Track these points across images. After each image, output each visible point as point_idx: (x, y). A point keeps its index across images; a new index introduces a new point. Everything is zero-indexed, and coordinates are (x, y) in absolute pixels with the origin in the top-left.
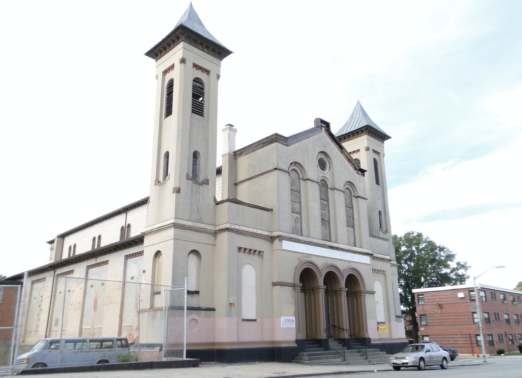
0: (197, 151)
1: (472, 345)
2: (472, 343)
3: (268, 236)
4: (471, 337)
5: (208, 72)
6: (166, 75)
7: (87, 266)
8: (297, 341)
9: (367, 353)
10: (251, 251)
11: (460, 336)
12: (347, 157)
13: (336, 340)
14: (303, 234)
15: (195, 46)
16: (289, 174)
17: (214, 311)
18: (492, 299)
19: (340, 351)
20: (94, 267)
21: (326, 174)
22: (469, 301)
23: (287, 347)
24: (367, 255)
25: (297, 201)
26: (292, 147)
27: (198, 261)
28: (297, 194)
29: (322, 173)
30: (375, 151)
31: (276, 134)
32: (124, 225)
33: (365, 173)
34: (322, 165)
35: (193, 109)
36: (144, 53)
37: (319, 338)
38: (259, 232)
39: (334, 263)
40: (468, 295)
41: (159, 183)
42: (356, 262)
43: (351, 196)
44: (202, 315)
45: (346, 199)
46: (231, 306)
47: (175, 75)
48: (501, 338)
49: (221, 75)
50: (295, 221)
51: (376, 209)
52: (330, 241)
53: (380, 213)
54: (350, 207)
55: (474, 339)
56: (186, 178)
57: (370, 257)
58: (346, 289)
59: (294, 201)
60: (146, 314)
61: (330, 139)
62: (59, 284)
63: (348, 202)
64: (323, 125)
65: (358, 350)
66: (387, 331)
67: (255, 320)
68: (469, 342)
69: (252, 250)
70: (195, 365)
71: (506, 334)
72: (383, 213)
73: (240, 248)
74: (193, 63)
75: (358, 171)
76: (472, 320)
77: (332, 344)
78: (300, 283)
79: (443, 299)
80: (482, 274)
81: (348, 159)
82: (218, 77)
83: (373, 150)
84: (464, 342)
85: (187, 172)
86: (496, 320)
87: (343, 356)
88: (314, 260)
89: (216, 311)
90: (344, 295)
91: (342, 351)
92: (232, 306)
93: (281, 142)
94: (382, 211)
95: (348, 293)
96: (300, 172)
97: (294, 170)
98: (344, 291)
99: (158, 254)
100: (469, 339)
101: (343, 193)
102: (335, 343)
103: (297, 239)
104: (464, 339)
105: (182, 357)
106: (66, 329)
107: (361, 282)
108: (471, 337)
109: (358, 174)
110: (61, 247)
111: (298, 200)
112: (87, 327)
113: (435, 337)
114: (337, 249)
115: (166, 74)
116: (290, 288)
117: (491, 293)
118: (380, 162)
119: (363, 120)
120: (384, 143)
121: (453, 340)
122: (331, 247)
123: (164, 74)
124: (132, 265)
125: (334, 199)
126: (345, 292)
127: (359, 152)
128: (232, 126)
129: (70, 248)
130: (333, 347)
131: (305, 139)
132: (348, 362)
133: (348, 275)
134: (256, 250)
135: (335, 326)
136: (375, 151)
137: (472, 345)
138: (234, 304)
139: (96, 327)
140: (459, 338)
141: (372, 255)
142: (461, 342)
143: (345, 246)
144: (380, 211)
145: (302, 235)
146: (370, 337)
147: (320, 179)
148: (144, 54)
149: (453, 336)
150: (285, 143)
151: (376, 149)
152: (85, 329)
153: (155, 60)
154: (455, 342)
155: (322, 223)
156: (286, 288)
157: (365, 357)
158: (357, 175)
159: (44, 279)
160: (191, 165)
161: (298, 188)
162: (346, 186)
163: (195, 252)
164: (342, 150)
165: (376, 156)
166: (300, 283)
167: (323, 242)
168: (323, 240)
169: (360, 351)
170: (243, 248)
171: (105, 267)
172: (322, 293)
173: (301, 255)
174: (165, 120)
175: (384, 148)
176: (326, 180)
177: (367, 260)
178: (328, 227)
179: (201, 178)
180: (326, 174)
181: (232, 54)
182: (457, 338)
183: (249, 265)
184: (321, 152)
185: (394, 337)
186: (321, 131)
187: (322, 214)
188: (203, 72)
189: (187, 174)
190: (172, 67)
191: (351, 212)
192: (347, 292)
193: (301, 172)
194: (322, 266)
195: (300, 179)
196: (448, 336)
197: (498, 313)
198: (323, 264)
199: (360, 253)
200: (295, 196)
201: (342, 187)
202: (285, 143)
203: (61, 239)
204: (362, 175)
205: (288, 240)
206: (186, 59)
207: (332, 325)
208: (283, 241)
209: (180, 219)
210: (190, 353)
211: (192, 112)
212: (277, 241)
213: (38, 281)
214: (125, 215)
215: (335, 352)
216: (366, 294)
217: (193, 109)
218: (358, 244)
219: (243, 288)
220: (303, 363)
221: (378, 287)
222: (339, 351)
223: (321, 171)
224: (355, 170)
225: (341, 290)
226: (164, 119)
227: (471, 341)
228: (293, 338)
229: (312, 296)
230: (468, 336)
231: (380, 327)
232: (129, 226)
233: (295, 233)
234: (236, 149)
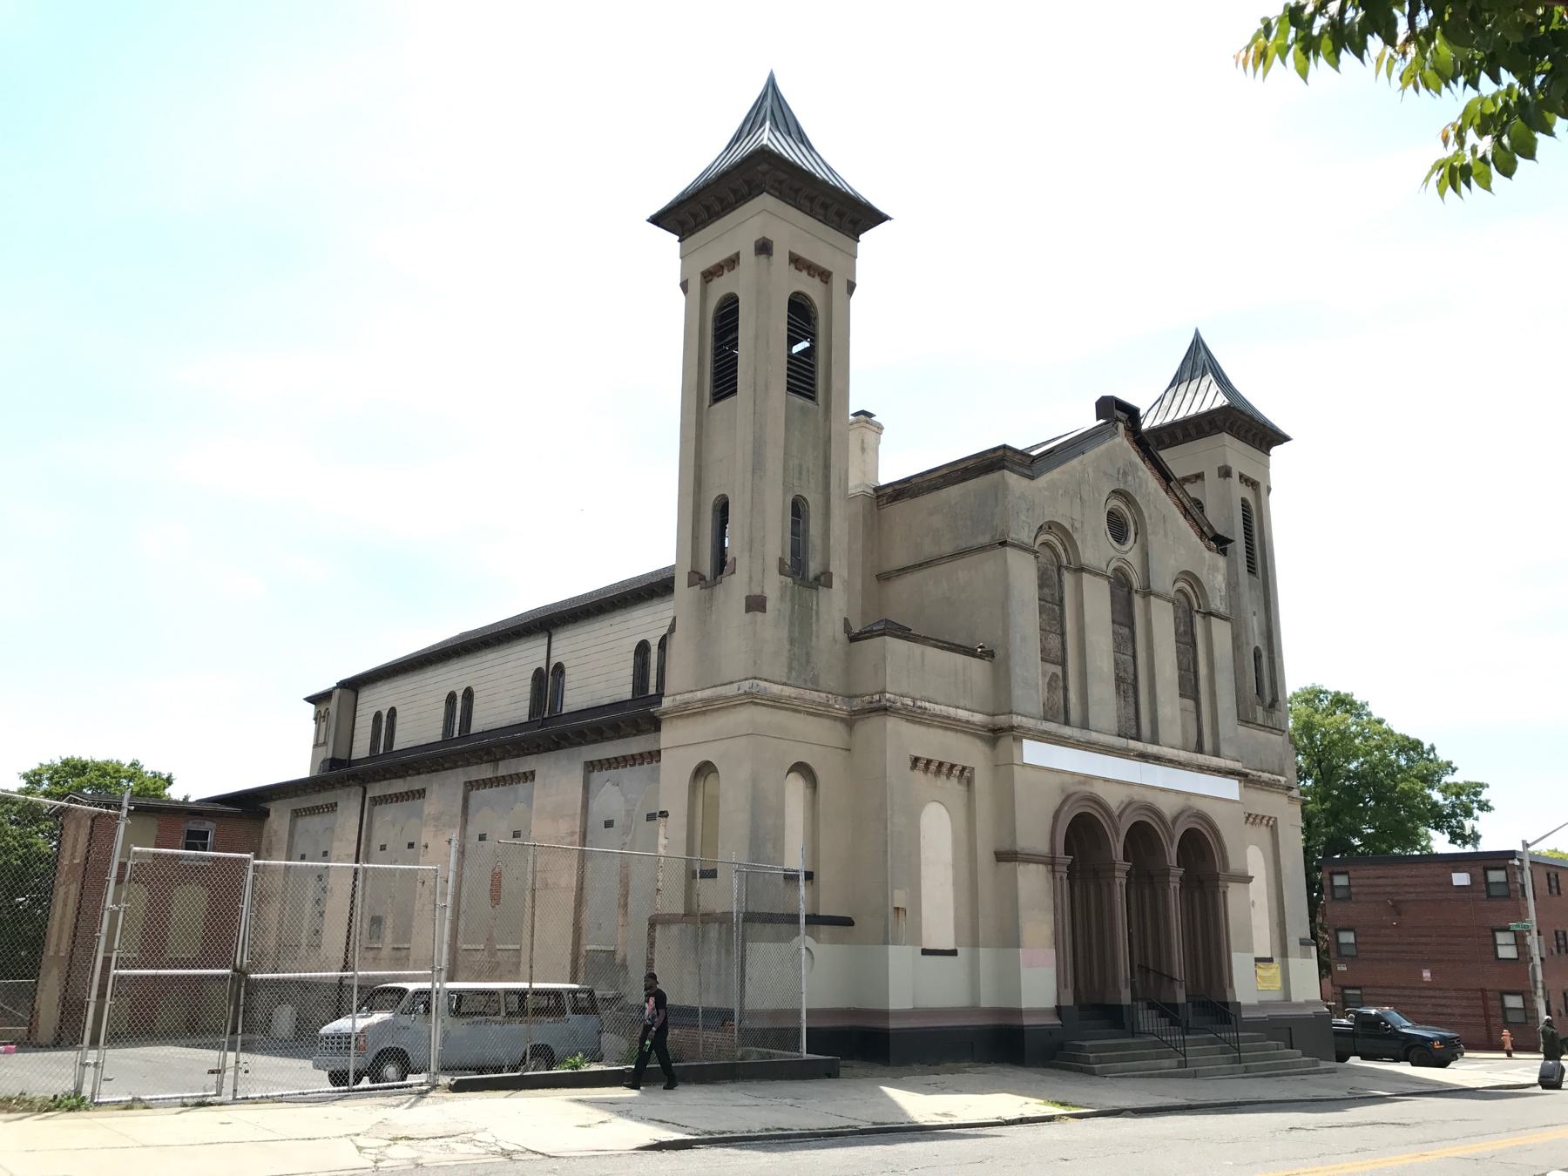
0: (802, 497)
1: (1488, 1022)
2: (1487, 1016)
3: (983, 727)
4: (1484, 998)
6: (710, 284)
7: (465, 783)
8: (1059, 1010)
9: (1238, 1043)
12: (1181, 502)
14: (1071, 719)
15: (793, 203)
16: (1037, 557)
17: (850, 927)
18: (1550, 892)
19: (1173, 1038)
20: (489, 785)
21: (1127, 552)
22: (1484, 896)
24: (1233, 777)
25: (1053, 630)
27: (808, 791)
28: (1053, 610)
31: (1005, 447)
32: (543, 665)
34: (1118, 527)
37: (841, 946)
38: (963, 714)
39: (1150, 797)
40: (1481, 879)
41: (700, 580)
42: (1205, 796)
43: (1191, 613)
44: (822, 936)
45: (1177, 620)
46: (898, 917)
49: (857, 282)
50: (1049, 684)
51: (1248, 644)
52: (1138, 738)
53: (1257, 656)
54: (1186, 640)
55: (1497, 1003)
57: (1240, 781)
60: (675, 929)
61: (1138, 452)
62: (377, 824)
63: (1182, 629)
64: (1119, 414)
66: (1278, 984)
67: (953, 953)
70: (830, 1073)
72: (1264, 654)
74: (790, 252)
75: (1209, 539)
76: (1492, 949)
77: (1147, 1019)
78: (1066, 855)
79: (1407, 889)
80: (1551, 833)
81: (1182, 509)
82: (851, 287)
83: (1241, 476)
86: (1559, 951)
88: (1100, 790)
89: (855, 927)
91: (1173, 1038)
93: (1016, 468)
94: (1261, 648)
96: (1062, 551)
97: (1044, 544)
99: (704, 770)
100: (1480, 1002)
101: (1171, 604)
103: (1058, 736)
104: (1464, 1003)
105: (797, 1049)
106: (406, 946)
107: (1218, 855)
108: (1484, 998)
109: (1209, 549)
110: (352, 714)
111: (1056, 628)
112: (469, 947)
113: (1380, 991)
114: (1158, 759)
115: (711, 280)
116: (1042, 867)
117: (1548, 875)
118: (1259, 508)
121: (1433, 1005)
122: (1144, 757)
123: (705, 278)
124: (604, 788)
126: (1178, 880)
127: (1199, 482)
128: (869, 415)
129: (378, 716)
130: (1146, 1025)
131: (1075, 457)
132: (1195, 1071)
133: (1185, 832)
134: (956, 765)
135: (1148, 970)
136: (1244, 479)
138: (904, 910)
139: (498, 947)
140: (1450, 998)
141: (1246, 775)
142: (1457, 1011)
143: (1176, 752)
145: (1067, 723)
146: (1238, 1000)
148: (648, 220)
149: (1431, 993)
152: (466, 950)
153: (678, 238)
154: (1439, 1010)
157: (1235, 1057)
158: (1207, 554)
159: (332, 807)
160: (789, 535)
162: (1181, 584)
164: (1168, 484)
165: (1248, 493)
166: (1066, 855)
167: (1121, 742)
168: (1119, 736)
170: (924, 759)
171: (522, 788)
172: (1121, 882)
173: (1067, 778)
174: (713, 407)
175: (1269, 468)
176: (1127, 568)
177: (1229, 789)
178: (1131, 700)
179: (814, 568)
180: (1127, 552)
181: (887, 223)
182: (1445, 998)
183: (938, 805)
185: (1295, 999)
186: (1115, 434)
188: (813, 276)
190: (733, 262)
191: (1191, 656)
193: (1065, 550)
194: (1119, 806)
196: (1417, 993)
198: (1122, 802)
199: (1214, 771)
200: (1049, 615)
202: (1029, 473)
203: (349, 694)
204: (1218, 553)
205: (1036, 738)
206: (772, 242)
207: (1139, 966)
208: (1024, 740)
209: (766, 680)
210: (818, 1039)
211: (788, 389)
212: (1006, 742)
213: (313, 811)
214: (546, 641)
215: (1156, 1041)
216: (1229, 884)
218: (1208, 744)
219: (923, 867)
221: (1255, 860)
222: (1169, 1038)
223: (1115, 543)
224: (1201, 538)
226: (709, 406)
227: (1485, 1007)
231: (1259, 971)
232: (559, 669)
233: (1049, 718)
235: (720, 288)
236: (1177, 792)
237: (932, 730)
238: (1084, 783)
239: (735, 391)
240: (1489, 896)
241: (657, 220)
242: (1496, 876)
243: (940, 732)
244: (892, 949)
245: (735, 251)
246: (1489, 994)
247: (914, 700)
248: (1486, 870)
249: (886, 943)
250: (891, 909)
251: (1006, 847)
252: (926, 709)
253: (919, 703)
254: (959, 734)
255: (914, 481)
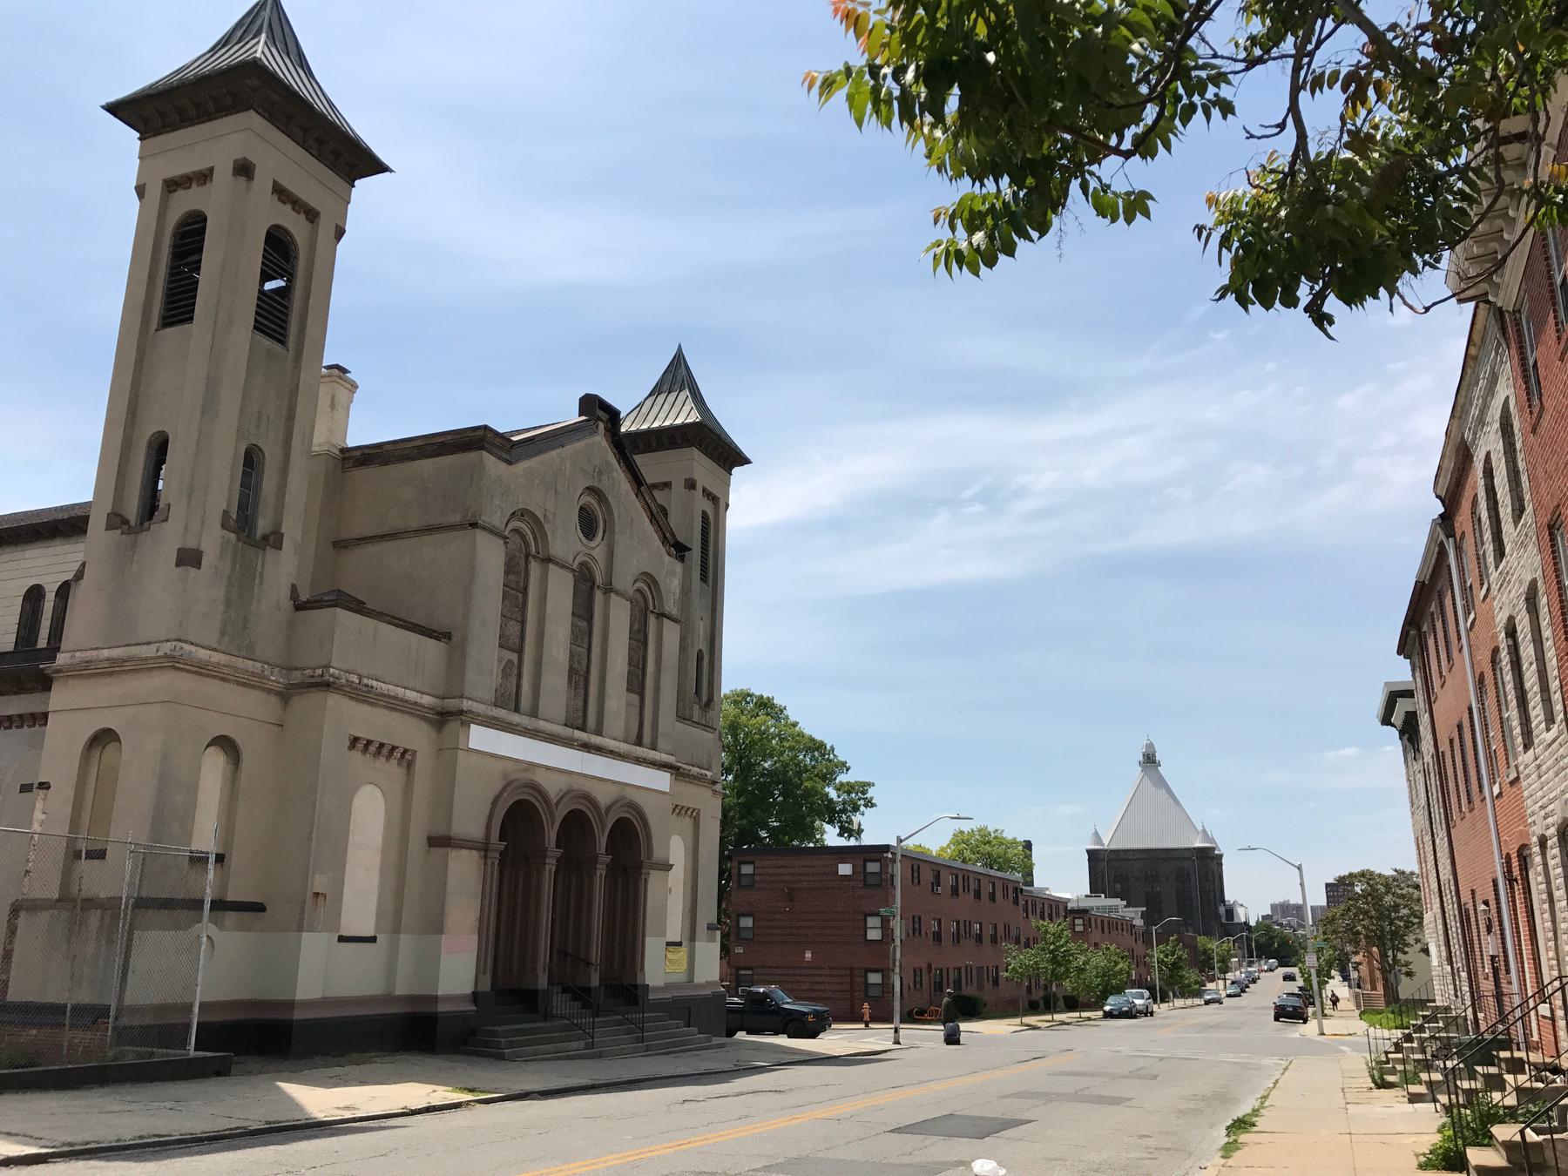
1: (852, 995)
3: (432, 709)
4: (852, 975)
5: (312, 215)
8: (475, 997)
10: (382, 750)
11: (828, 972)
13: (564, 991)
16: (506, 543)
21: (593, 548)
22: (861, 885)
23: (316, 1020)
26: (521, 467)
29: (585, 546)
30: (707, 494)
31: (486, 427)
33: (687, 553)
34: (588, 524)
35: (259, 319)
36: (104, 104)
38: (411, 695)
39: (588, 787)
47: (212, 201)
48: (918, 979)
52: (583, 728)
54: (639, 639)
56: (219, 526)
58: (559, 852)
59: (509, 615)
64: (601, 413)
65: (620, 1017)
67: (373, 939)
68: (848, 987)
69: (386, 746)
70: (219, 1070)
71: (929, 966)
73: (355, 741)
77: (561, 1003)
83: (704, 490)
84: (837, 987)
85: (224, 507)
86: (914, 934)
87: (589, 1034)
88: (541, 778)
90: (601, 874)
92: (321, 899)
93: (494, 450)
94: (704, 650)
95: (611, 867)
98: (602, 863)
102: (560, 999)
108: (852, 975)
114: (599, 750)
115: (175, 191)
119: (695, 411)
120: (354, 186)
122: (587, 747)
125: (606, 618)
127: (666, 490)
128: (345, 371)
131: (554, 448)
136: (707, 494)
137: (852, 995)
141: (677, 769)
143: (617, 743)
144: (700, 651)
145: (517, 710)
147: (580, 559)
148: (103, 107)
150: (505, 456)
151: (710, 489)
155: (570, 678)
156: (465, 852)
158: (667, 558)
161: (522, 584)
162: (640, 585)
163: (225, 743)
164: (639, 489)
167: (567, 732)
168: (566, 725)
169: (627, 1019)
170: (364, 739)
173: (510, 765)
177: (661, 781)
178: (581, 691)
179: (263, 525)
180: (593, 548)
184: (587, 488)
186: (595, 432)
187: (572, 655)
188: (284, 203)
189: (226, 514)
190: (205, 176)
191: (641, 654)
192: (501, 854)
195: (531, 558)
197: (920, 918)
201: (497, 519)
202: (505, 456)
211: (255, 327)
212: (453, 725)
217: (259, 319)
218: (647, 738)
220: (500, 1057)
221: (676, 850)
223: (583, 538)
225: (594, 860)
228: (467, 988)
229: (574, 878)
230: (848, 972)
231: (669, 955)
234: (353, 441)
235: (186, 201)
236: (613, 782)
237: (376, 710)
238: (526, 770)
239: (192, 318)
240: (866, 885)
241: (115, 109)
242: (873, 867)
243: (386, 712)
244: (305, 934)
245: (209, 165)
246: (856, 972)
247: (360, 677)
248: (865, 861)
249: (300, 929)
250: (309, 894)
251: (441, 831)
252: (372, 687)
253: (365, 681)
254: (405, 716)
255: (386, 448)
